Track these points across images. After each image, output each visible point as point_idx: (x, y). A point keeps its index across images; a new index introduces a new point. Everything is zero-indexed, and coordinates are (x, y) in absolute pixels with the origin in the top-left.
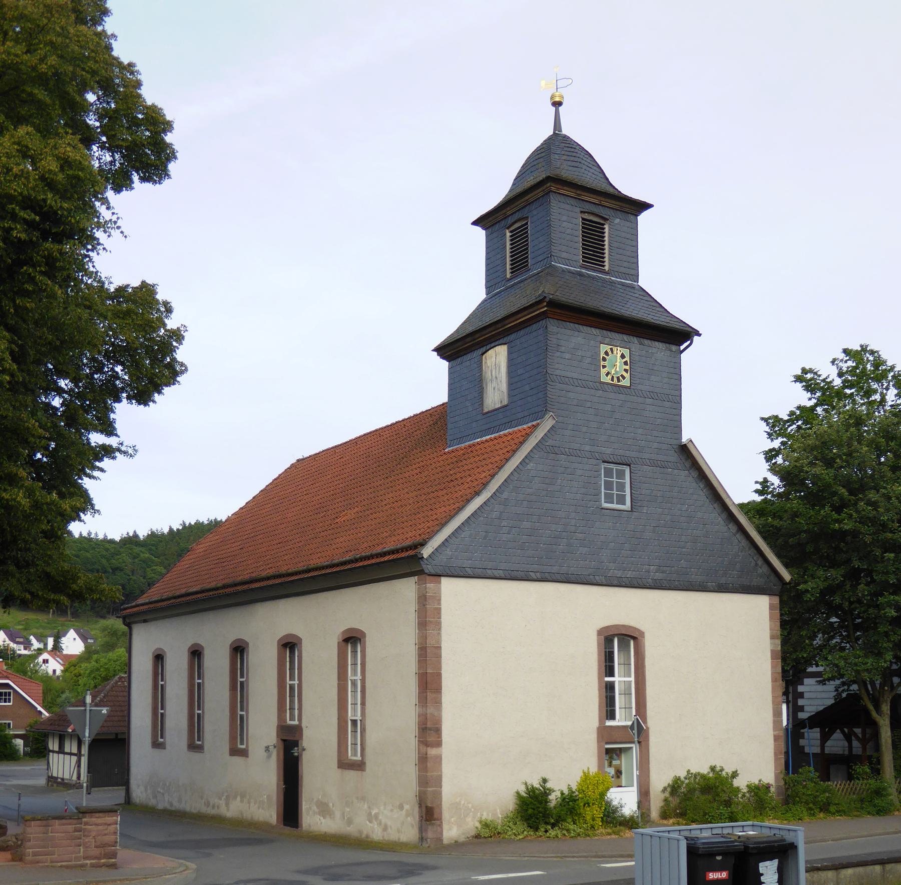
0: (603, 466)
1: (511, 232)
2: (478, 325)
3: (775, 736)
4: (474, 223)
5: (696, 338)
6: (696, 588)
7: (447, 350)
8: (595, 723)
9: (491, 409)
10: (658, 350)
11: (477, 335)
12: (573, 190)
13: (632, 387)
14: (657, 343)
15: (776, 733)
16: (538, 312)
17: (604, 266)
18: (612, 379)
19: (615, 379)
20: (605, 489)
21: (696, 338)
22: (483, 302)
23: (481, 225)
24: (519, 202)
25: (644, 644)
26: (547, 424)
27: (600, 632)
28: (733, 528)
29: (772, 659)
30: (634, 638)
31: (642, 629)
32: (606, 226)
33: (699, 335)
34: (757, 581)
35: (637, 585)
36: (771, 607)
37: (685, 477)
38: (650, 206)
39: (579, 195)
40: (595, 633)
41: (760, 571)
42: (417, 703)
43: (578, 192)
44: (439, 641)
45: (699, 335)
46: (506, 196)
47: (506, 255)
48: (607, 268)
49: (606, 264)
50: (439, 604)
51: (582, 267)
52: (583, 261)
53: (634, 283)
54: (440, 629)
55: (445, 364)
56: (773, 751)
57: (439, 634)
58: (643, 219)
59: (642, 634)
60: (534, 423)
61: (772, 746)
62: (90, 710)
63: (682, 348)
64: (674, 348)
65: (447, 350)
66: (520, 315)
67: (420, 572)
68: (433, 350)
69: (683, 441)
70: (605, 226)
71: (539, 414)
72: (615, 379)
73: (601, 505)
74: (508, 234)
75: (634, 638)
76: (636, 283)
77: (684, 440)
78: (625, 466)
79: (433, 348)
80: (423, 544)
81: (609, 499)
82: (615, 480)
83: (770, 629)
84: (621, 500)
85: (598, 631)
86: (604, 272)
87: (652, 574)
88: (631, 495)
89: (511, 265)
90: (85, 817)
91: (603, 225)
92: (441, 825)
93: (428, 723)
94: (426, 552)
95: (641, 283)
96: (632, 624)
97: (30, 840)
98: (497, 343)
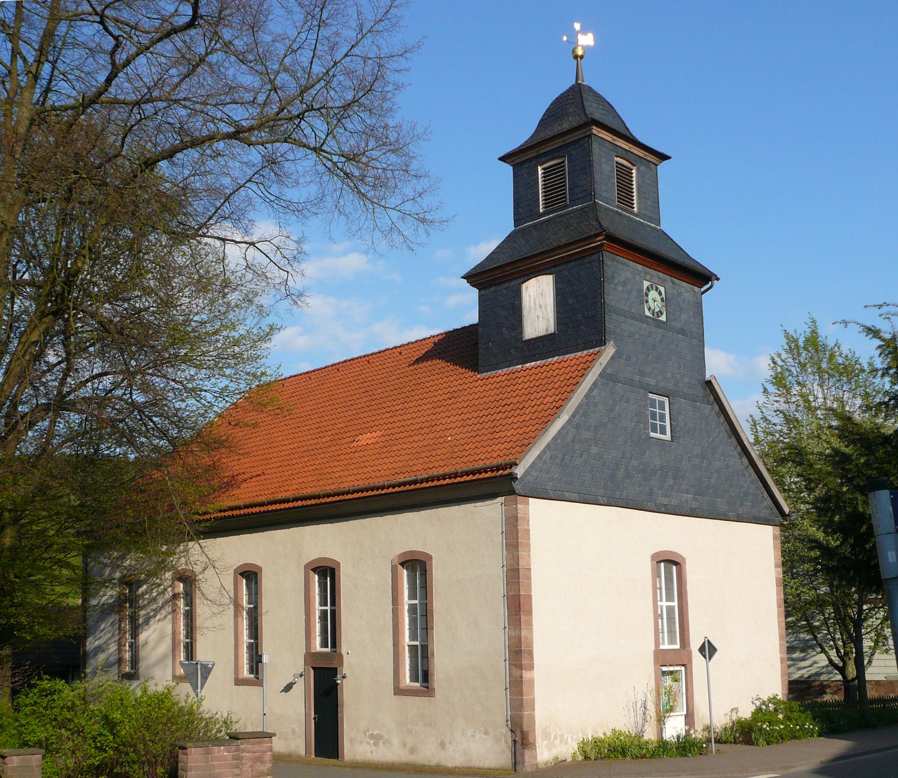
1: (543, 169)
2: (504, 259)
3: (781, 659)
4: (500, 159)
8: (653, 648)
10: (685, 288)
11: (519, 264)
12: (610, 135)
13: (668, 323)
16: (595, 244)
17: (633, 208)
19: (655, 314)
23: (507, 161)
24: (556, 141)
26: (609, 350)
28: (746, 461)
30: (676, 563)
32: (634, 171)
33: (718, 279)
34: (765, 513)
35: (678, 513)
37: (709, 410)
39: (615, 140)
42: (507, 626)
43: (614, 137)
44: (529, 563)
45: (718, 279)
48: (635, 209)
50: (528, 525)
51: (618, 207)
54: (529, 551)
55: (475, 292)
57: (529, 556)
58: (663, 167)
60: (597, 349)
61: (779, 668)
63: (703, 289)
64: (696, 289)
66: (571, 247)
67: (512, 492)
68: (463, 278)
69: (707, 377)
75: (676, 563)
77: (708, 377)
79: (462, 275)
84: (663, 432)
88: (671, 426)
89: (545, 200)
90: (242, 744)
91: (632, 170)
93: (523, 646)
94: (519, 471)
95: (665, 226)
97: (191, 770)
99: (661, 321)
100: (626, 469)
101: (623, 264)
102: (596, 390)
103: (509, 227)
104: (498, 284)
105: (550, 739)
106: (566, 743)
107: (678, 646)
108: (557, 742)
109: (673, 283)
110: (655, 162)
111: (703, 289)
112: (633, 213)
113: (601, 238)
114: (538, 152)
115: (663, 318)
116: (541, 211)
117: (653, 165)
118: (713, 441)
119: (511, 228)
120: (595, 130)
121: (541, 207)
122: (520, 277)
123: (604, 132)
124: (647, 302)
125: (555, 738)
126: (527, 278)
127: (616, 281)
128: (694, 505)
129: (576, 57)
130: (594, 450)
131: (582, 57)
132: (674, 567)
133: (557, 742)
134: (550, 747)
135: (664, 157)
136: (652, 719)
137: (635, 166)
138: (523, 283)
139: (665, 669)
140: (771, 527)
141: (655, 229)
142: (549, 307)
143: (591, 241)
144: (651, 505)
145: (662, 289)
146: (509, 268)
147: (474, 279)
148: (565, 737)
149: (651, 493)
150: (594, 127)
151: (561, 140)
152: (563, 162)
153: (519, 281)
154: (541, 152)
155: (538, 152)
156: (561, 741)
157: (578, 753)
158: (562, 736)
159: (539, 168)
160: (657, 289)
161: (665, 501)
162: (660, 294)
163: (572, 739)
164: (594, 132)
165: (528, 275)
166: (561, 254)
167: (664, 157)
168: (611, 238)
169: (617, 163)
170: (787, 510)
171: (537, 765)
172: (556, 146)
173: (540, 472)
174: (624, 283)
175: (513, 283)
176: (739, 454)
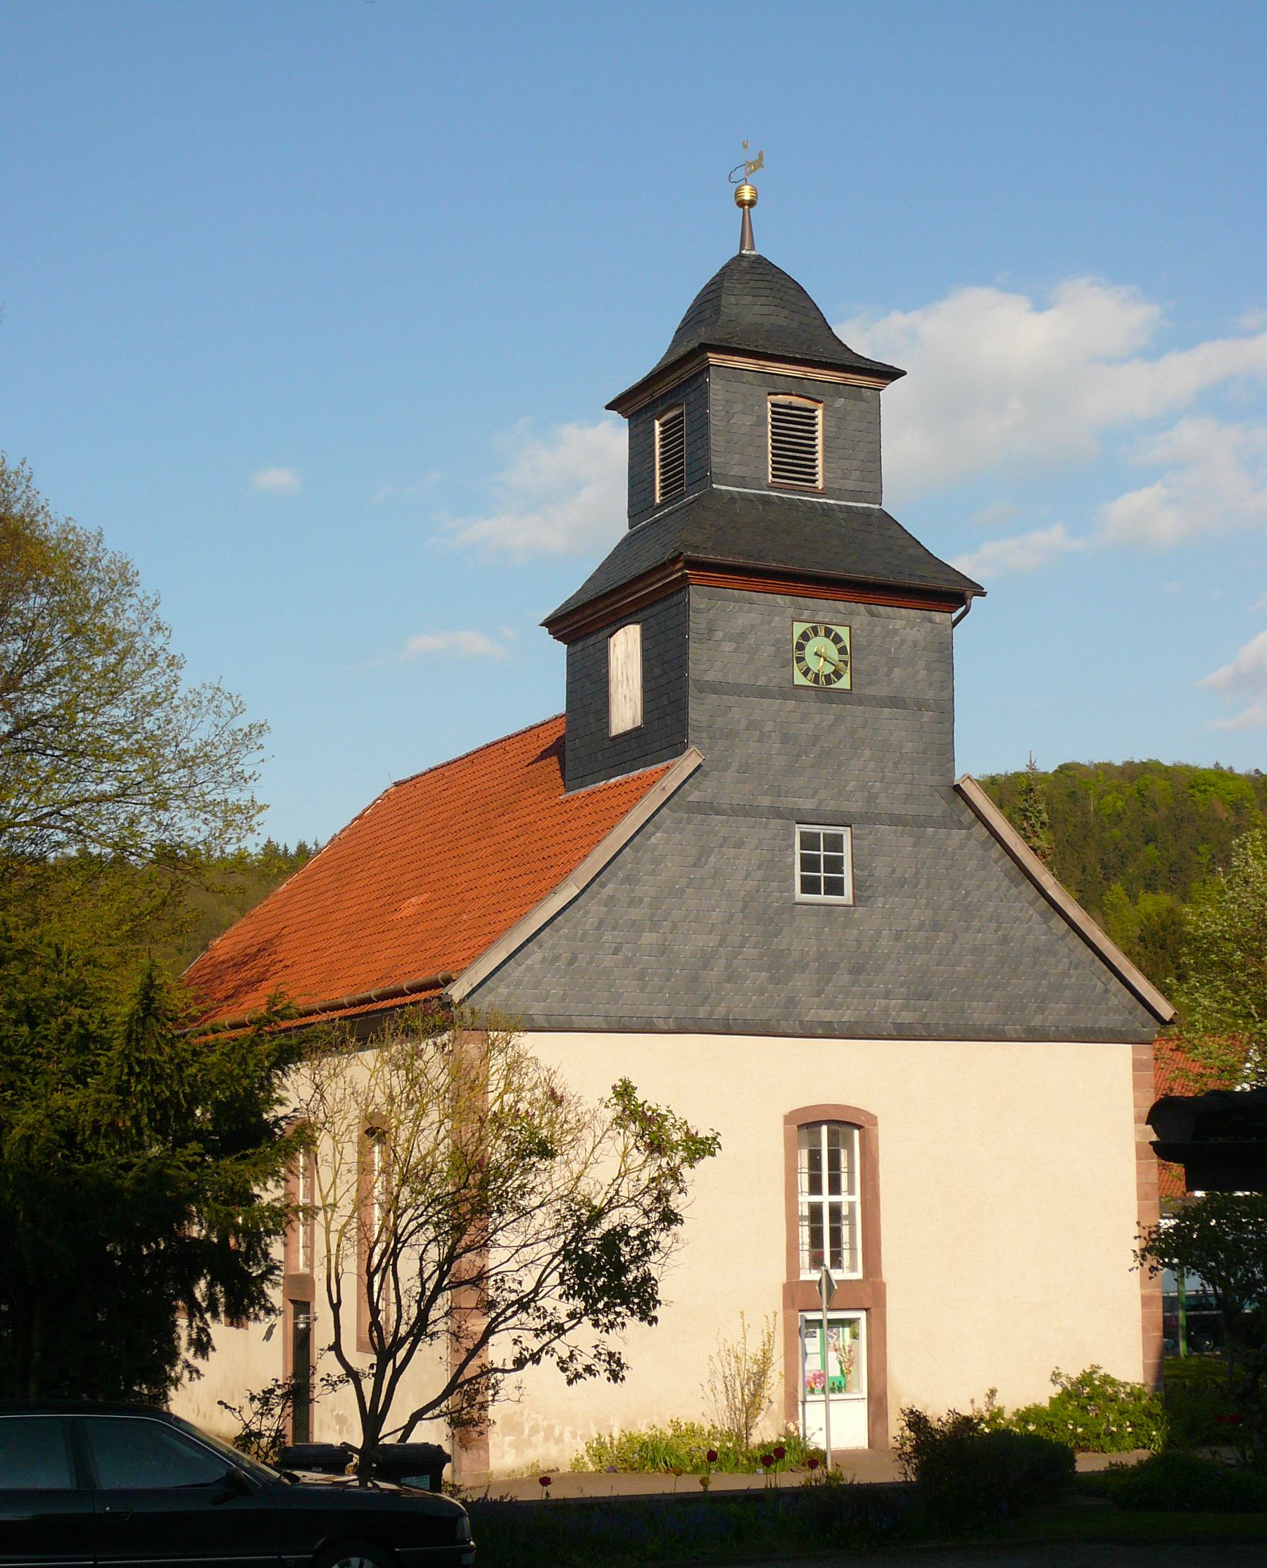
0: (799, 829)
3: (1143, 1297)
4: (609, 407)
5: (976, 601)
6: (983, 1036)
7: (562, 625)
8: (783, 1278)
9: (620, 731)
13: (854, 691)
14: (903, 611)
15: (1147, 1291)
18: (816, 680)
19: (822, 680)
20: (802, 870)
21: (976, 601)
22: (625, 540)
25: (877, 1135)
26: (688, 762)
27: (788, 1119)
29: (1138, 1158)
30: (859, 1127)
31: (873, 1111)
32: (819, 413)
36: (1137, 1066)
38: (902, 373)
40: (782, 1120)
41: (1114, 1001)
43: (761, 363)
46: (663, 359)
47: (654, 464)
48: (820, 484)
49: (819, 477)
52: (774, 476)
53: (872, 506)
55: (562, 648)
56: (1140, 1324)
58: (891, 393)
59: (873, 1120)
62: (830, 1309)
65: (562, 625)
68: (542, 625)
70: (816, 413)
71: (678, 748)
72: (822, 680)
73: (794, 897)
74: (658, 428)
76: (877, 506)
78: (841, 828)
79: (541, 622)
80: (448, 981)
81: (810, 886)
82: (822, 853)
83: (1135, 1106)
84: (835, 887)
85: (785, 1117)
86: (815, 493)
87: (893, 1013)
91: (813, 411)
92: (487, 1451)
94: (457, 992)
96: (853, 1103)
98: (632, 620)
99: (842, 691)
100: (728, 965)
101: (736, 600)
102: (658, 835)
103: (622, 529)
104: (589, 635)
105: (522, 1433)
106: (559, 1441)
107: (859, 1275)
108: (539, 1438)
109: (872, 614)
110: (872, 385)
111: (955, 616)
112: (815, 493)
113: (679, 566)
114: (652, 395)
115: (844, 683)
116: (658, 501)
117: (869, 393)
118: (967, 895)
119: (625, 530)
120: (714, 359)
121: (658, 493)
122: (606, 627)
123: (736, 358)
124: (800, 660)
125: (534, 1431)
126: (614, 628)
127: (720, 635)
128: (907, 1017)
129: (741, 204)
130: (649, 938)
131: (752, 203)
132: (856, 1132)
133: (539, 1438)
134: (519, 1447)
135: (892, 374)
136: (775, 1406)
137: (820, 402)
138: (611, 636)
139: (811, 1316)
140: (1130, 1046)
141: (868, 513)
142: (635, 680)
143: (668, 571)
144: (785, 1026)
145: (844, 632)
146: (579, 617)
147: (557, 628)
148: (557, 1432)
149: (791, 1002)
150: (709, 354)
151: (674, 376)
152: (681, 415)
153: (601, 636)
154: (657, 395)
155: (652, 395)
156: (547, 1438)
157: (586, 1459)
158: (550, 1428)
159: (657, 423)
160: (828, 633)
161: (827, 1015)
162: (837, 640)
163: (574, 1435)
164: (712, 361)
165: (614, 623)
166: (652, 584)
167: (892, 374)
168: (693, 564)
169: (773, 405)
170: (1166, 1011)
171: (489, 1475)
172: (671, 386)
173: (517, 986)
174: (739, 638)
175: (592, 640)
176: (1041, 914)
